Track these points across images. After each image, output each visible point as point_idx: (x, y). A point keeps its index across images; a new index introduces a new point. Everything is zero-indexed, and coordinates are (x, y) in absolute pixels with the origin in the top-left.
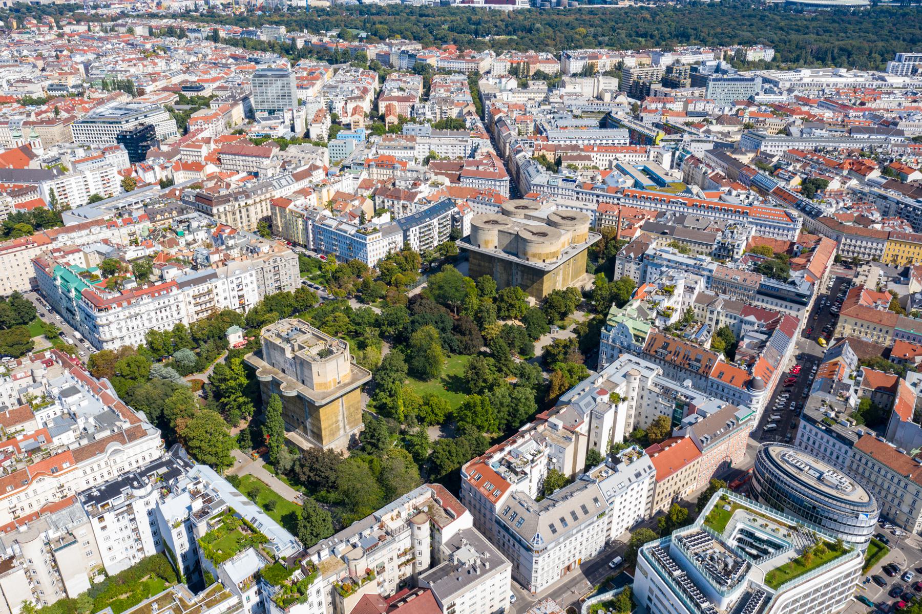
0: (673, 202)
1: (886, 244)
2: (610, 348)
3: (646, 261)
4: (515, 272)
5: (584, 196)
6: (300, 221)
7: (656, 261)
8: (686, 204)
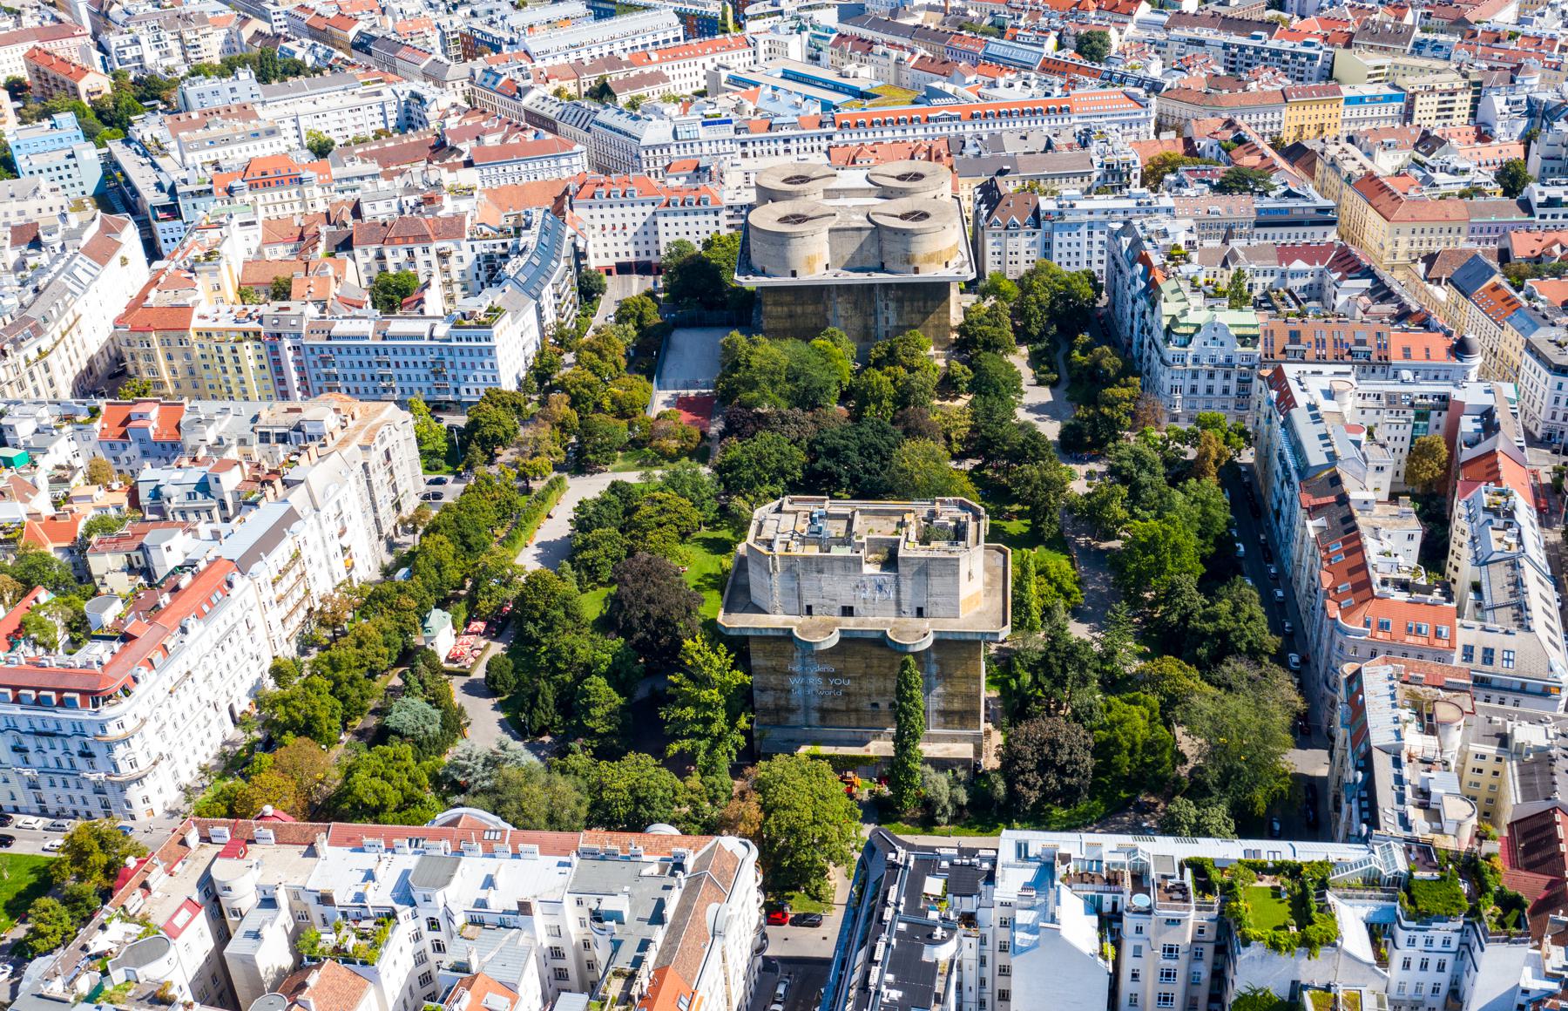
0: (936, 120)
1: (1285, 110)
2: (1189, 376)
3: (1046, 225)
4: (880, 304)
5: (758, 148)
6: (248, 351)
7: (1068, 219)
8: (959, 118)
